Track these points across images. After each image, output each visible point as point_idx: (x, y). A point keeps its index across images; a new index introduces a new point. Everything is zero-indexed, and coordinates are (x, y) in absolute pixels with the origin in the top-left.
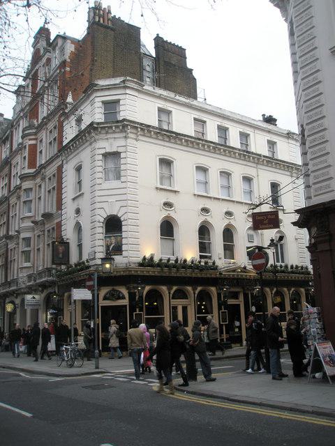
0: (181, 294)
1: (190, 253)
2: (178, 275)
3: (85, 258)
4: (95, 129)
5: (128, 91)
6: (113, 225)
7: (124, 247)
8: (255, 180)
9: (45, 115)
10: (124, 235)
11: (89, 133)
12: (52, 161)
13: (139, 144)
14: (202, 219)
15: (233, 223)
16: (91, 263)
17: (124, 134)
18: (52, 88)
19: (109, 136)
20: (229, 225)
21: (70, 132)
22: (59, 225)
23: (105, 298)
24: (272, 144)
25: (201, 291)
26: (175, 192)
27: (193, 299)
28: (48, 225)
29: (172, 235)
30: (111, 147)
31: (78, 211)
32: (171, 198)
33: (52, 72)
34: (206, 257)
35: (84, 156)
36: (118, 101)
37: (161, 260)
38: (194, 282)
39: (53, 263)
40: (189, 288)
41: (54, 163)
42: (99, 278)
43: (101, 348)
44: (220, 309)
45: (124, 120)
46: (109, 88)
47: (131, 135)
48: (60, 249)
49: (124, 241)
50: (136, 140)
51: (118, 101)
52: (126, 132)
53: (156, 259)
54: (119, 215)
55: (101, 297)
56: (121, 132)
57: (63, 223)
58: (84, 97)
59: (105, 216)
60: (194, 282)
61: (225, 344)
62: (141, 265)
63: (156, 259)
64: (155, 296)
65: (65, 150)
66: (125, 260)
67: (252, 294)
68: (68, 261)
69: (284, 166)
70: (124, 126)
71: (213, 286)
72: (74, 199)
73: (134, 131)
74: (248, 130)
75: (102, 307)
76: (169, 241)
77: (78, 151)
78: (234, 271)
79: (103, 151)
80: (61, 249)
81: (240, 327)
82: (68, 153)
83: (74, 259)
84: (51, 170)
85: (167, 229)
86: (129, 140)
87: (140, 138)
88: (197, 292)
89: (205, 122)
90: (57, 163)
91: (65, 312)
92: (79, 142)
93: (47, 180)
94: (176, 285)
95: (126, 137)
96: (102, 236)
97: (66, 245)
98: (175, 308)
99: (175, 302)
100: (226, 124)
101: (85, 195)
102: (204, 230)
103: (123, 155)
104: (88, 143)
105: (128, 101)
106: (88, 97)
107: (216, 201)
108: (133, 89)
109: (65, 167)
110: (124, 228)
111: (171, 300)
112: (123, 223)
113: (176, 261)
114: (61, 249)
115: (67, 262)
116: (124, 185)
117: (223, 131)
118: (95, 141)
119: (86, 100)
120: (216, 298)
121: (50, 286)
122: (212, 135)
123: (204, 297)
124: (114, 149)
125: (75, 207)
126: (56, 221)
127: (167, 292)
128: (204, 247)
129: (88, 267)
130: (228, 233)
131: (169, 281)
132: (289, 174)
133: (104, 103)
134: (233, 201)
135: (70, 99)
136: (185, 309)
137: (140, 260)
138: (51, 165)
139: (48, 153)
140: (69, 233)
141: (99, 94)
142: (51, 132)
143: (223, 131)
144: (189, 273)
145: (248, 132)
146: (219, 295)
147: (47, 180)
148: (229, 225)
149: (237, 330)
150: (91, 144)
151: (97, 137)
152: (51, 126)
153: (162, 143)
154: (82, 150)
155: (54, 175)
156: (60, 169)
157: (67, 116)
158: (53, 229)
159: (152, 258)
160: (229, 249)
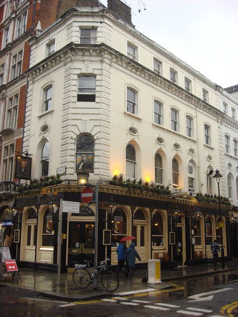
0: (140, 215)
1: (148, 176)
2: (141, 196)
3: (52, 172)
4: (72, 49)
5: (106, 21)
6: (86, 142)
7: (96, 165)
8: (194, 120)
9: (10, 41)
11: (65, 54)
12: (16, 82)
13: (112, 70)
14: (158, 147)
16: (62, 178)
17: (100, 59)
18: (19, 19)
19: (85, 58)
20: (160, 150)
21: (39, 54)
22: (20, 142)
24: (205, 92)
25: (138, 210)
28: (6, 142)
30: (87, 69)
31: (45, 128)
32: (136, 125)
33: (20, 6)
35: (57, 76)
36: (94, 29)
37: (128, 181)
38: (152, 204)
39: (16, 177)
40: (128, 207)
41: (17, 84)
42: (100, 194)
44: (169, 231)
45: (103, 44)
46: (87, 15)
47: (106, 60)
48: (23, 166)
49: (96, 159)
50: (110, 65)
51: (94, 29)
52: (102, 56)
53: (125, 179)
54: (92, 134)
56: (98, 55)
57: (25, 139)
58: (60, 21)
59: (78, 133)
60: (152, 204)
61: (172, 263)
62: (111, 183)
63: (125, 179)
64: (121, 213)
65: (29, 72)
66: (97, 178)
67: (173, 217)
68: (30, 176)
69: (214, 112)
70: (102, 49)
71: (165, 209)
72: (40, 117)
73: (109, 57)
74: (191, 77)
76: (132, 164)
77: (48, 72)
78: (181, 197)
79: (79, 72)
80: (24, 163)
81: (181, 248)
82: (35, 74)
83: (36, 173)
84: (16, 89)
85: (131, 152)
86: (104, 65)
87: (113, 64)
88: (135, 212)
89: (161, 63)
90: (23, 83)
91: (23, 225)
92: (52, 63)
93: (7, 100)
94: (138, 206)
95: (102, 61)
96: (74, 152)
97: (28, 160)
98: (134, 229)
99: (136, 221)
100: (176, 68)
101: (54, 113)
102: (159, 157)
103: (98, 77)
104: (62, 64)
105: (104, 30)
106: (65, 22)
107: (168, 133)
108: (109, 19)
109: (30, 87)
110: (96, 147)
113: (140, 182)
114: (24, 163)
115: (28, 177)
116: (98, 106)
117: (173, 73)
118: (71, 61)
119: (61, 25)
120: (167, 221)
121: (6, 200)
122: (166, 74)
123: (158, 218)
124: (90, 71)
125: (42, 123)
126: (16, 138)
127: (149, 213)
128: (159, 173)
130: (176, 162)
131: (133, 202)
132: (216, 119)
133: (82, 29)
134: (180, 135)
135: (39, 27)
136: (142, 228)
137: (111, 178)
138: (13, 87)
139: (10, 76)
140: (31, 147)
141: (77, 19)
142: (15, 57)
143: (173, 73)
144: (145, 195)
145: (191, 79)
146: (169, 217)
147: (7, 100)
148: (160, 150)
149: (179, 250)
150: (65, 65)
151: (73, 58)
152: (15, 51)
153: (130, 73)
154: (53, 71)
155: (16, 96)
156: (24, 90)
157: (37, 40)
158: (12, 145)
159: (121, 178)
160: (176, 179)
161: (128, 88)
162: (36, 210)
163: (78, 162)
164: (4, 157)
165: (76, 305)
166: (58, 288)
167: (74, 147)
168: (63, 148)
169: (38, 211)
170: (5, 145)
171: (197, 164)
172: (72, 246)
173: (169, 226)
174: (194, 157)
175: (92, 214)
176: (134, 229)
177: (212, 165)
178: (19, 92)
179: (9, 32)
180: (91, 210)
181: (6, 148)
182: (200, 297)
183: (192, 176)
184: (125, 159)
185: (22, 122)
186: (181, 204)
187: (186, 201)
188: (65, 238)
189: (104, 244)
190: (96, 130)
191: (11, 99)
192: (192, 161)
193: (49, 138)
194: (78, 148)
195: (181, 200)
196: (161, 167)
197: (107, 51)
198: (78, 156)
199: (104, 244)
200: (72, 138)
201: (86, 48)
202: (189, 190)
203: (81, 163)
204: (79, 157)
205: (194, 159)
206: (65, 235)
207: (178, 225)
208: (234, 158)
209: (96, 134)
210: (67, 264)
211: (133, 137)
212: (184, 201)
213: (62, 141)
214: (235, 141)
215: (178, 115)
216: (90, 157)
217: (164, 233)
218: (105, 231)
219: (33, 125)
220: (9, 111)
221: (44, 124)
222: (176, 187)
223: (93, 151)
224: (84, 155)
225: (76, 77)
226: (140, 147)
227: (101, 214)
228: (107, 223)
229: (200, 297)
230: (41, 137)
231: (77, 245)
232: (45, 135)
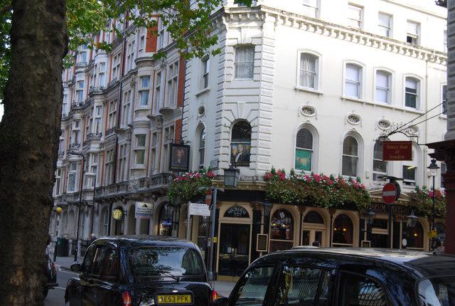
14: (349, 128)
22: (180, 124)
23: (227, 215)
25: (340, 216)
26: (318, 94)
31: (202, 110)
32: (313, 102)
49: (252, 151)
54: (249, 120)
59: (233, 120)
66: (251, 173)
88: (304, 214)
99: (306, 226)
103: (257, 49)
110: (253, 136)
112: (253, 130)
126: (176, 119)
127: (329, 215)
128: (349, 164)
140: (190, 135)
147: (168, 68)
155: (176, 64)
161: (380, 13)
164: (153, 146)
170: (166, 127)
172: (223, 250)
175: (247, 215)
178: (179, 59)
179: (108, 82)
180: (246, 211)
181: (167, 129)
184: (295, 147)
185: (181, 101)
190: (254, 114)
191: (171, 67)
193: (206, 124)
194: (234, 137)
201: (242, 11)
206: (215, 238)
210: (217, 271)
215: (391, 79)
216: (247, 147)
217: (354, 242)
219: (192, 106)
220: (170, 82)
225: (232, 50)
226: (320, 134)
227: (257, 215)
231: (230, 250)
232: (202, 120)
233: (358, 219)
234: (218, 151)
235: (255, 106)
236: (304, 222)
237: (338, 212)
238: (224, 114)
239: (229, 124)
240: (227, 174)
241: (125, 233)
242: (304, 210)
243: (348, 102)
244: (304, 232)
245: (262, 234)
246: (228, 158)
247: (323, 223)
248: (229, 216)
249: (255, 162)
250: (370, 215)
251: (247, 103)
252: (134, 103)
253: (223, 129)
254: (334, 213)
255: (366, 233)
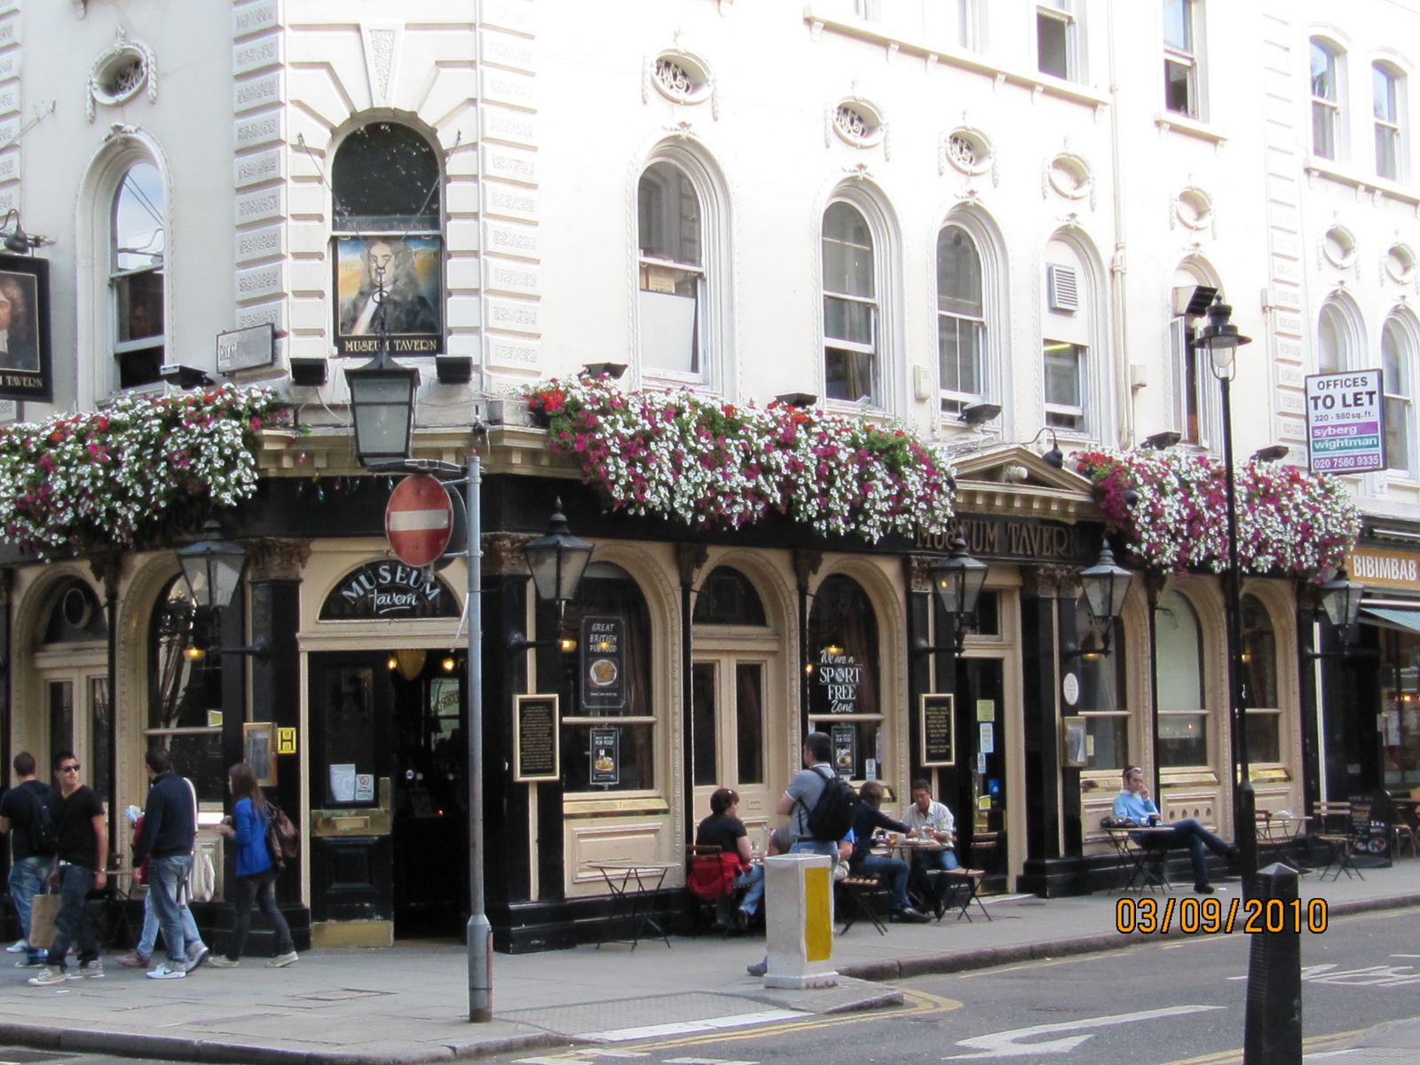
10: (456, 235)
15: (704, 132)
20: (858, 185)
23: (335, 607)
25: (720, 570)
26: (1214, 140)
27: (793, 624)
29: (688, 247)
34: (1069, 421)
43: (306, 900)
44: (917, 683)
49: (456, 273)
55: (310, 601)
59: (340, 116)
75: (313, 656)
78: (992, 474)
88: (814, 582)
98: (701, 682)
110: (455, 197)
111: (694, 628)
112: (453, 166)
127: (790, 582)
129: (307, 432)
136: (749, 676)
148: (858, 185)
162: (100, 589)
163: (347, 296)
165: (284, 809)
166: (346, 688)
167: (322, 199)
168: (244, 246)
169: (112, 596)
171: (1106, 253)
173: (916, 658)
174: (1081, 209)
175: (447, 606)
176: (701, 682)
177: (1210, 253)
182: (1015, 1041)
183: (1069, 332)
186: (993, 519)
187: (1028, 499)
188: (287, 749)
189: (519, 778)
190: (457, 84)
192: (1070, 235)
195: (991, 496)
196: (866, 285)
197: (394, 220)
198: (345, 256)
199: (519, 778)
200: (300, 147)
202: (1056, 419)
203: (364, 295)
204: (351, 259)
205: (1087, 223)
206: (287, 732)
207: (975, 647)
208: (1370, 190)
209: (450, 115)
210: (306, 900)
211: (682, 114)
212: (1009, 498)
213: (240, 122)
214: (1388, 72)
218: (524, 704)
221: (118, 46)
222: (974, 416)
223: (435, 224)
224: (380, 250)
228: (531, 655)
229: (1015, 1041)
230: (103, 130)
233: (900, 596)
234: (275, 278)
235: (457, 45)
236: (698, 620)
237: (716, 555)
238: (290, 84)
239: (321, 138)
240: (364, 396)
241: (565, 719)
242: (700, 559)
243: (1392, 203)
244: (697, 666)
245: (531, 694)
246: (322, 315)
247: (761, 621)
248: (355, 614)
249: (474, 330)
250: (963, 570)
251: (408, 26)
252: (1360, 372)
253: (289, 163)
254: (814, 568)
255: (531, 655)
